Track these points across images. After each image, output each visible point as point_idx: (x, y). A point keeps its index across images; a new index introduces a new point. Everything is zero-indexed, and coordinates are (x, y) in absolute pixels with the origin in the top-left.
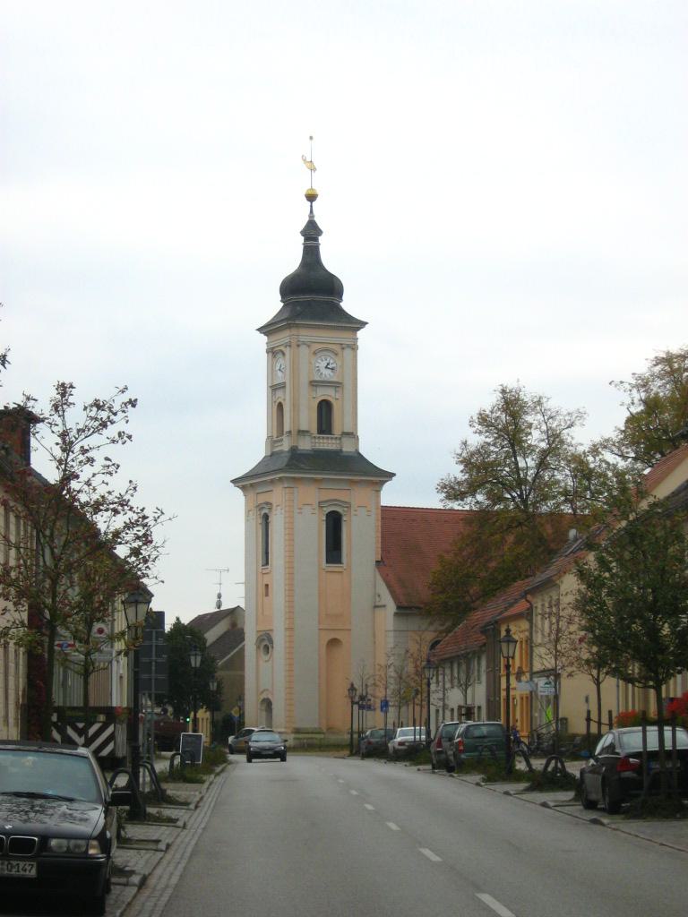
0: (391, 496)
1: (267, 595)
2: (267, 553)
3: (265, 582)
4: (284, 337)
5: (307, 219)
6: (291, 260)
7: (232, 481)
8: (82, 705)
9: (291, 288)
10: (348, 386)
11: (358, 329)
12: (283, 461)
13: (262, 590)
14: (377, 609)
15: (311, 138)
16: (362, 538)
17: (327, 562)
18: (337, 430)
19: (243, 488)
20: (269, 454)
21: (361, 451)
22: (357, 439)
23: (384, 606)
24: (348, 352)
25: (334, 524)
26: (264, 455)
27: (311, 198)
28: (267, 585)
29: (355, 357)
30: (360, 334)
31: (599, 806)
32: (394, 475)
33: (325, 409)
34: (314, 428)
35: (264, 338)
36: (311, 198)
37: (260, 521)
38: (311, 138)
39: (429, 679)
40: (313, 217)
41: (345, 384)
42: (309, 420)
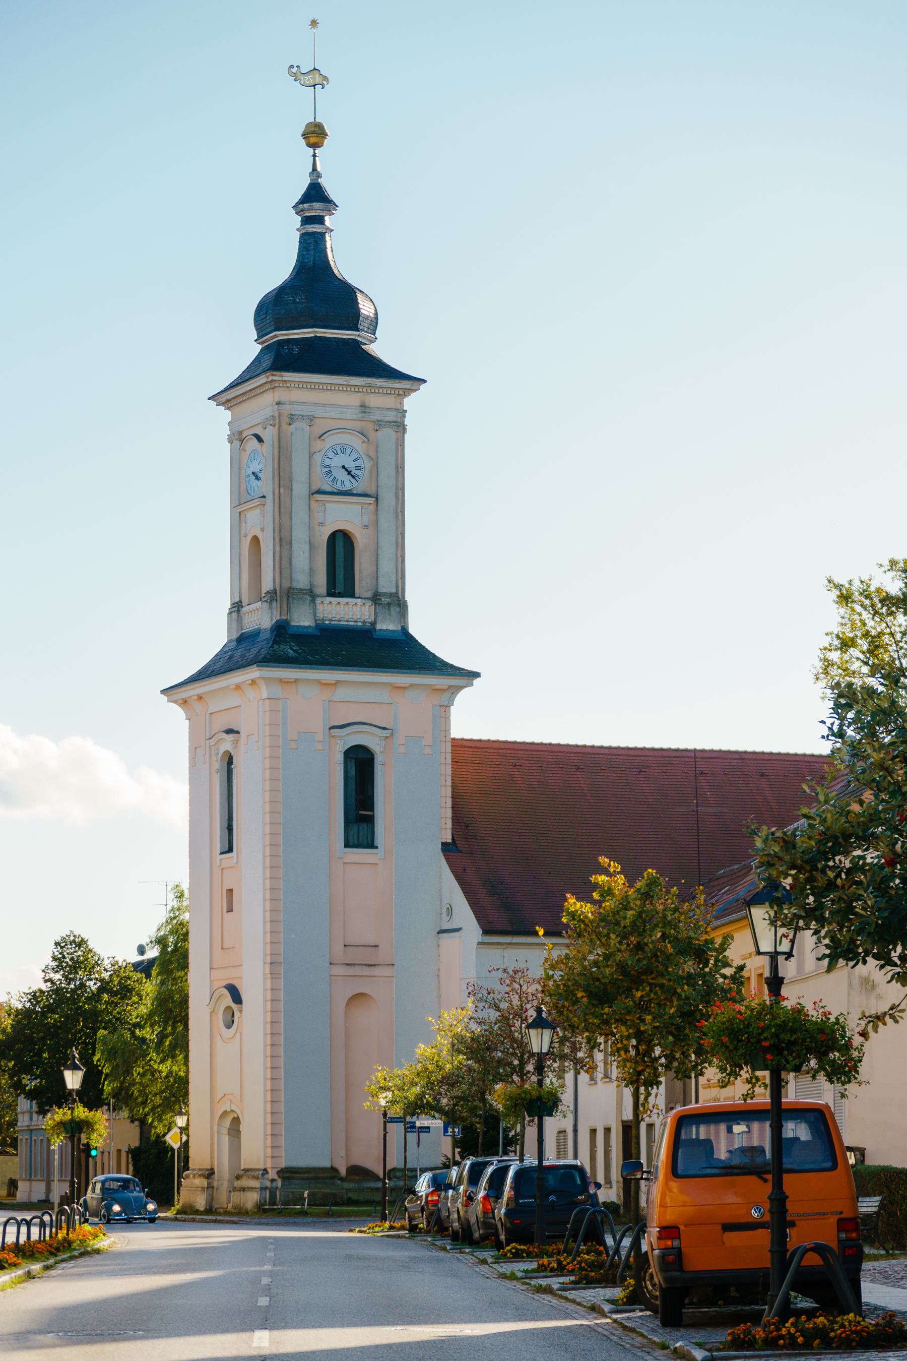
0: (476, 717)
1: (230, 910)
2: (230, 829)
3: (226, 888)
4: (261, 407)
5: (306, 182)
6: (279, 266)
7: (164, 692)
8: (784, 1166)
9: (274, 311)
10: (387, 497)
11: (407, 392)
12: (261, 647)
13: (220, 901)
14: (441, 935)
15: (314, 23)
16: (417, 809)
17: (347, 845)
18: (362, 584)
19: (184, 703)
20: (235, 636)
21: (412, 630)
22: (404, 430)
23: (459, 930)
24: (387, 434)
25: (360, 767)
26: (225, 641)
27: (315, 135)
28: (230, 891)
29: (400, 445)
30: (409, 403)
31: (182, 1074)
32: (477, 675)
33: (341, 546)
34: (321, 581)
35: (225, 415)
36: (315, 135)
37: (217, 765)
38: (314, 23)
39: (774, 956)
40: (319, 176)
41: (380, 487)
42: (310, 566)
